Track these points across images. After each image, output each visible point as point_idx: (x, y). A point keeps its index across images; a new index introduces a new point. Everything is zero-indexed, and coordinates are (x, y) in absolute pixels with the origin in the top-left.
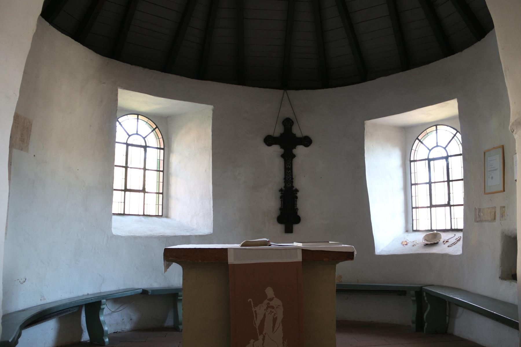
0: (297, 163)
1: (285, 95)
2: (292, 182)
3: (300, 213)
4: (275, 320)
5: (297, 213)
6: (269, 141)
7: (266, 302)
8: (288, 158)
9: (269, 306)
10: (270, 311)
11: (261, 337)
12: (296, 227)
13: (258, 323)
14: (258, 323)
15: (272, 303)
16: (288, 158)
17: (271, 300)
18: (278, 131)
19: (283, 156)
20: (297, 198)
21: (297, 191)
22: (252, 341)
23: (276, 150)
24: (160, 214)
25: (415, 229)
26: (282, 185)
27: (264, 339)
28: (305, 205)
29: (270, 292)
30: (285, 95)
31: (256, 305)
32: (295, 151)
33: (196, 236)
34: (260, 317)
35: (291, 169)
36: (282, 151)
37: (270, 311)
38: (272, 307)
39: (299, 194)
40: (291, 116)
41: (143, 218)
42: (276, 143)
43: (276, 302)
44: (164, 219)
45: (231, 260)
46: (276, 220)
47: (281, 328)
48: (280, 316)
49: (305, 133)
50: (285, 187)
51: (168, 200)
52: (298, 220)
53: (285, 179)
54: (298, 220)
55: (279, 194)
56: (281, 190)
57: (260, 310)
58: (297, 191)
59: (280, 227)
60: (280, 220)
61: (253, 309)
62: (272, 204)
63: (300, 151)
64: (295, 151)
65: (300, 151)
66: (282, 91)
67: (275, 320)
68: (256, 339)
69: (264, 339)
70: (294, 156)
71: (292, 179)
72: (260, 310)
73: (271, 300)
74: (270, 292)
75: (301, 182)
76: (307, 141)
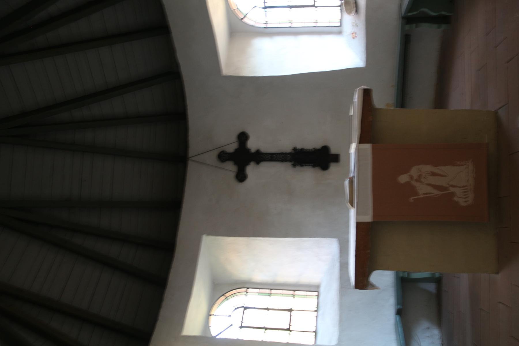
0: (267, 148)
1: (192, 159)
4: (433, 174)
5: (319, 150)
6: (241, 177)
7: (414, 183)
8: (259, 157)
10: (424, 180)
11: (452, 190)
12: (333, 151)
13: (436, 192)
14: (436, 192)
15: (415, 177)
16: (259, 157)
17: (411, 177)
18: (231, 168)
19: (258, 162)
21: (295, 149)
22: (456, 199)
23: (251, 170)
24: (316, 293)
26: (288, 165)
28: (310, 141)
29: (403, 179)
31: (416, 194)
37: (424, 180)
38: (420, 176)
39: (299, 147)
40: (216, 153)
41: (320, 312)
43: (414, 171)
44: (322, 290)
45: (368, 218)
46: (326, 172)
47: (443, 168)
48: (428, 168)
50: (290, 161)
52: (325, 149)
54: (325, 149)
55: (298, 168)
56: (294, 165)
57: (423, 189)
59: (333, 167)
60: (325, 167)
61: (422, 196)
62: (308, 175)
63: (252, 145)
65: (252, 145)
67: (433, 174)
68: (453, 194)
70: (258, 152)
72: (423, 189)
73: (411, 177)
74: (403, 179)
75: (286, 145)
76: (243, 137)
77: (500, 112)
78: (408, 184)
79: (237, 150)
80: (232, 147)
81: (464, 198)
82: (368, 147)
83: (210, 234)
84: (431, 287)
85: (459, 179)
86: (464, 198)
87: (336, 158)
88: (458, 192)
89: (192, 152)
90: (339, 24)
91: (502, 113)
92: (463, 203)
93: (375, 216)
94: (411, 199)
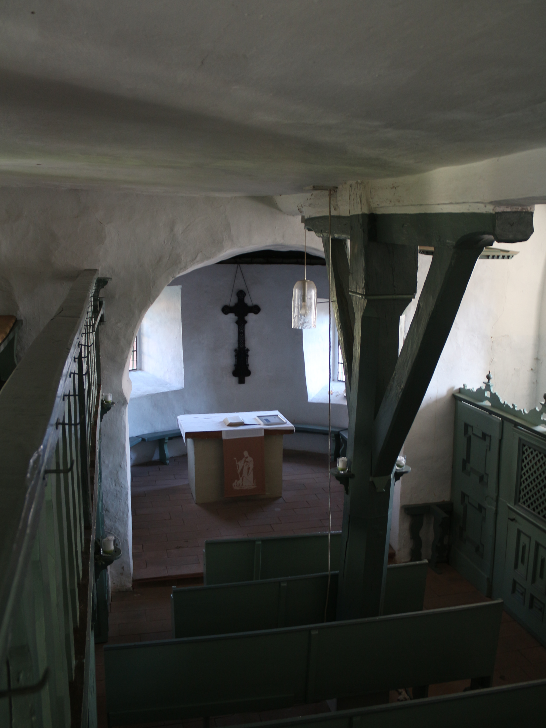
0: (248, 328)
1: (239, 269)
2: (244, 343)
3: (251, 368)
4: (249, 469)
5: (248, 368)
6: (226, 310)
7: (244, 459)
8: (241, 323)
9: (245, 461)
10: (246, 464)
11: (241, 479)
12: (247, 379)
13: (239, 470)
14: (239, 470)
15: (247, 460)
16: (241, 323)
17: (247, 458)
18: (232, 301)
19: (237, 322)
20: (248, 356)
22: (236, 481)
23: (232, 317)
24: (135, 368)
25: (339, 379)
26: (236, 346)
27: (242, 479)
28: (255, 361)
29: (246, 454)
30: (239, 269)
31: (238, 461)
32: (247, 318)
33: (172, 391)
34: (240, 468)
35: (244, 333)
36: (236, 318)
37: (246, 464)
38: (247, 462)
39: (250, 353)
40: (243, 288)
42: (231, 312)
43: (250, 459)
44: (139, 373)
45: (224, 437)
46: (231, 374)
47: (252, 473)
48: (252, 466)
49: (255, 302)
50: (239, 347)
51: (140, 355)
52: (248, 373)
53: (239, 341)
54: (248, 373)
55: (234, 353)
56: (235, 350)
57: (240, 464)
58: (248, 350)
59: (235, 379)
60: (235, 374)
61: (237, 464)
62: (228, 360)
64: (247, 318)
65: (251, 317)
66: (236, 265)
67: (249, 469)
68: (238, 479)
69: (242, 479)
71: (244, 341)
72: (240, 464)
73: (247, 458)
74: (246, 454)
75: (251, 343)
76: (256, 309)
77: (281, 499)
78: (243, 456)
79: (246, 305)
80: (248, 301)
81: (236, 485)
82: (263, 434)
83: (182, 289)
84: (156, 457)
85: (247, 482)
86: (236, 485)
87: (241, 381)
88: (240, 482)
89: (242, 265)
90: (339, 379)
91: (281, 500)
92: (234, 484)
93: (226, 440)
94: (235, 458)
